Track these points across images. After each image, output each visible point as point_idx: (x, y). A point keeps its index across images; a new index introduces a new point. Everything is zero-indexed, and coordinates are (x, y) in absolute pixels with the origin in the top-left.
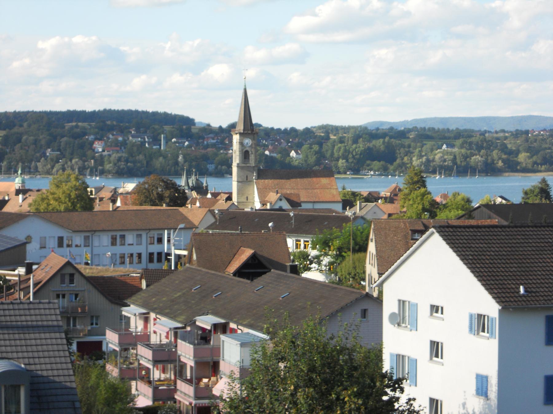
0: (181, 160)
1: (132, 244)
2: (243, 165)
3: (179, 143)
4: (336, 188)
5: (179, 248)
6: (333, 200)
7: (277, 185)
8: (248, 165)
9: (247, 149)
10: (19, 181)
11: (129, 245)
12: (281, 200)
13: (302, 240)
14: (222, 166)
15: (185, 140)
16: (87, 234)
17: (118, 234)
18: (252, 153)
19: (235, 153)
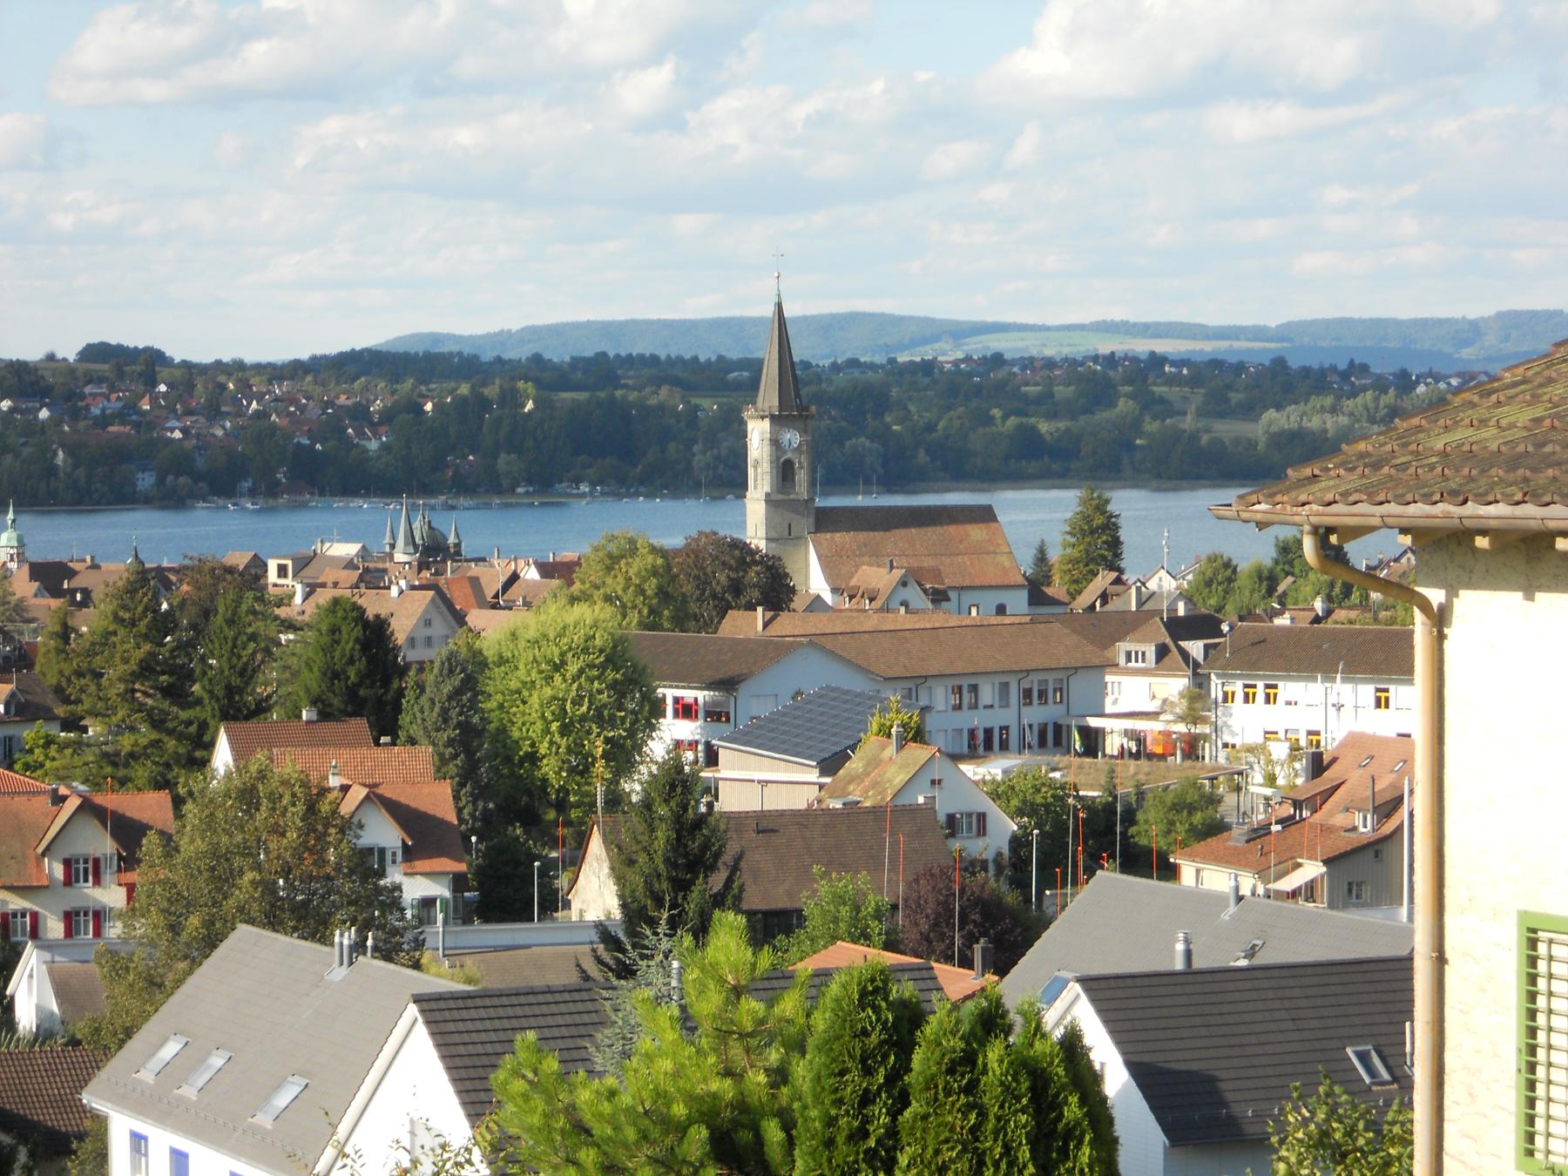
0: (65, 461)
1: (992, 706)
2: (780, 497)
3: (22, 412)
4: (1007, 550)
5: (1094, 712)
6: (1006, 582)
7: (865, 545)
8: (791, 497)
9: (789, 455)
10: (9, 540)
11: (985, 707)
12: (904, 584)
13: (1260, 685)
14: (178, 475)
15: (38, 405)
16: (1003, 679)
17: (965, 683)
18: (801, 467)
19: (755, 467)
